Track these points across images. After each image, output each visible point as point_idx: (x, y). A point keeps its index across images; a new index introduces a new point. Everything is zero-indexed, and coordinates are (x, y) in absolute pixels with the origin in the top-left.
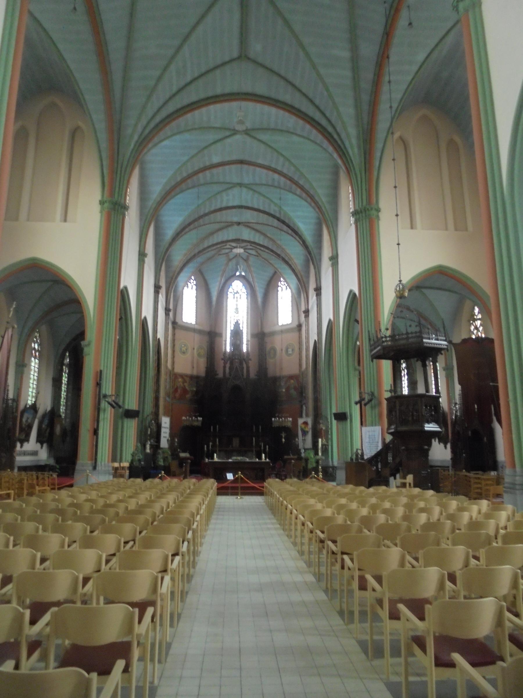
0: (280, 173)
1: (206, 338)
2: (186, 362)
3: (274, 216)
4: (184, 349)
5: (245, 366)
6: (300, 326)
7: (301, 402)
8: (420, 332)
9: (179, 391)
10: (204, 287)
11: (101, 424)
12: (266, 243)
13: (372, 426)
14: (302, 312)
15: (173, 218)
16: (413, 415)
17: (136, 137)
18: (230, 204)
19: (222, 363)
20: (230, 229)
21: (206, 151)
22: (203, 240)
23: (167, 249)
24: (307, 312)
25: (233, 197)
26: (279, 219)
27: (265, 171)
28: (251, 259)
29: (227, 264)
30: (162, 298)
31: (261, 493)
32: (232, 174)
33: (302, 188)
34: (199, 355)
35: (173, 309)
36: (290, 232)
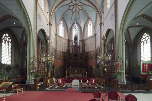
6: (96, 35)
9: (59, 56)
10: (66, 25)
28: (80, 12)
29: (72, 15)
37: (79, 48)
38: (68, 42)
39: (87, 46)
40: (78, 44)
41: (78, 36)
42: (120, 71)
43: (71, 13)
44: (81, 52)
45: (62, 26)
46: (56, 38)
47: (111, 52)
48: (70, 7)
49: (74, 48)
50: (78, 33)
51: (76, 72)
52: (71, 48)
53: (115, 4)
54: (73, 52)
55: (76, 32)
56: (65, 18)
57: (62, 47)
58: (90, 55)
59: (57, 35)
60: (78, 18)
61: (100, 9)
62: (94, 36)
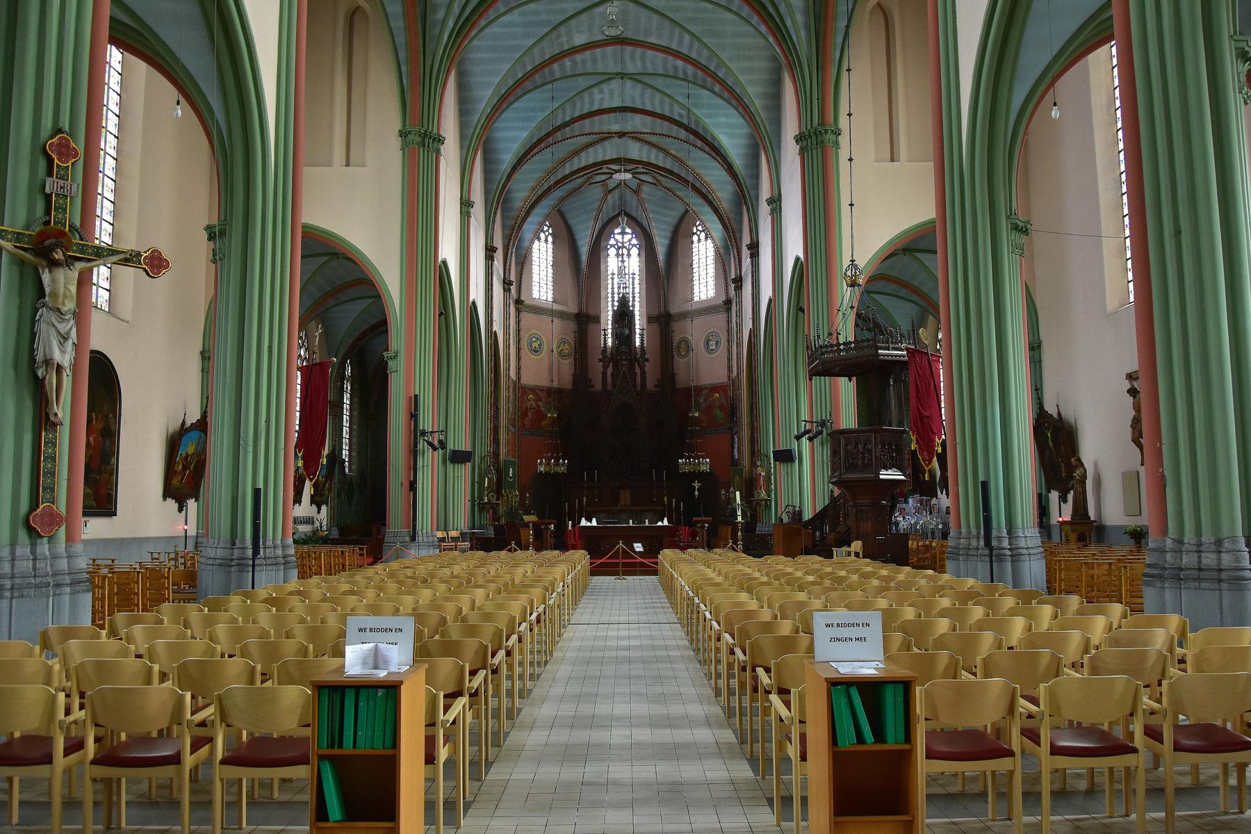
0: (686, 59)
1: (572, 326)
2: (539, 364)
3: (679, 124)
5: (638, 370)
7: (731, 429)
8: (874, 339)
10: (566, 240)
11: (420, 474)
12: (668, 163)
14: (730, 280)
15: (513, 135)
16: (863, 458)
17: (451, 23)
18: (606, 106)
20: (606, 143)
21: (562, 29)
22: (562, 162)
23: (505, 186)
24: (738, 281)
25: (611, 95)
26: (687, 128)
27: (660, 55)
29: (604, 199)
30: (498, 264)
31: (654, 572)
32: (607, 60)
33: (722, 83)
34: (561, 353)
35: (516, 282)
36: (707, 149)
40: (638, 343)
42: (763, 494)
43: (597, 191)
44: (650, 385)
49: (616, 367)
51: (628, 502)
52: (596, 368)
54: (609, 387)
55: (623, 267)
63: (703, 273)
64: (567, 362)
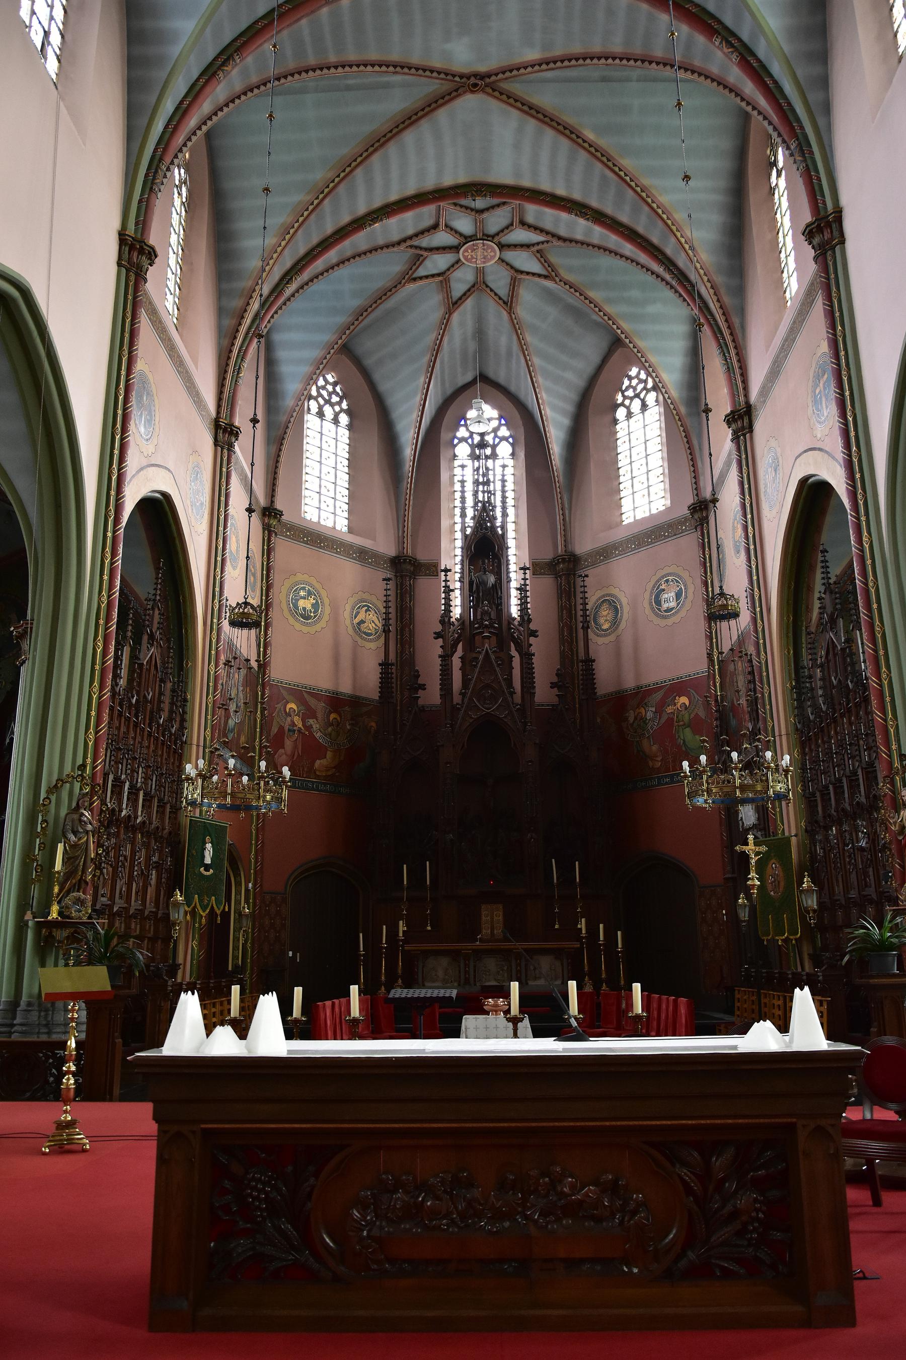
4: (306, 604)
6: (702, 510)
9: (288, 744)
10: (372, 415)
13: (335, 1039)
19: (436, 648)
28: (528, 298)
29: (445, 323)
37: (527, 657)
38: (391, 585)
39: (615, 623)
40: (515, 611)
41: (511, 527)
44: (544, 693)
45: (328, 426)
46: (268, 551)
47: (857, 705)
48: (417, 260)
49: (470, 646)
50: (510, 486)
51: (498, 932)
52: (429, 654)
53: (829, 297)
55: (484, 471)
56: (366, 346)
57: (326, 639)
58: (653, 726)
59: (277, 514)
60: (503, 340)
61: (722, 291)
62: (681, 522)
63: (639, 469)
64: (372, 645)
